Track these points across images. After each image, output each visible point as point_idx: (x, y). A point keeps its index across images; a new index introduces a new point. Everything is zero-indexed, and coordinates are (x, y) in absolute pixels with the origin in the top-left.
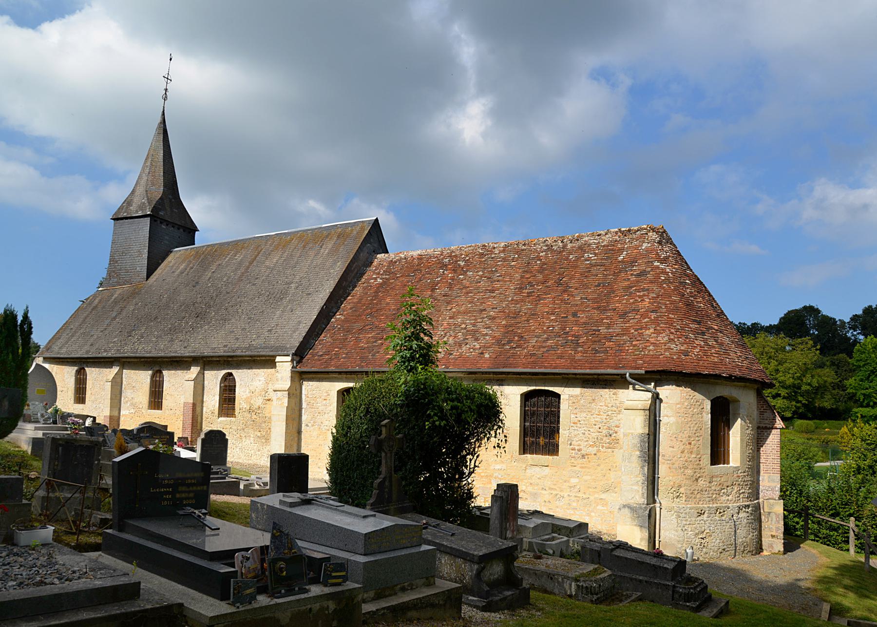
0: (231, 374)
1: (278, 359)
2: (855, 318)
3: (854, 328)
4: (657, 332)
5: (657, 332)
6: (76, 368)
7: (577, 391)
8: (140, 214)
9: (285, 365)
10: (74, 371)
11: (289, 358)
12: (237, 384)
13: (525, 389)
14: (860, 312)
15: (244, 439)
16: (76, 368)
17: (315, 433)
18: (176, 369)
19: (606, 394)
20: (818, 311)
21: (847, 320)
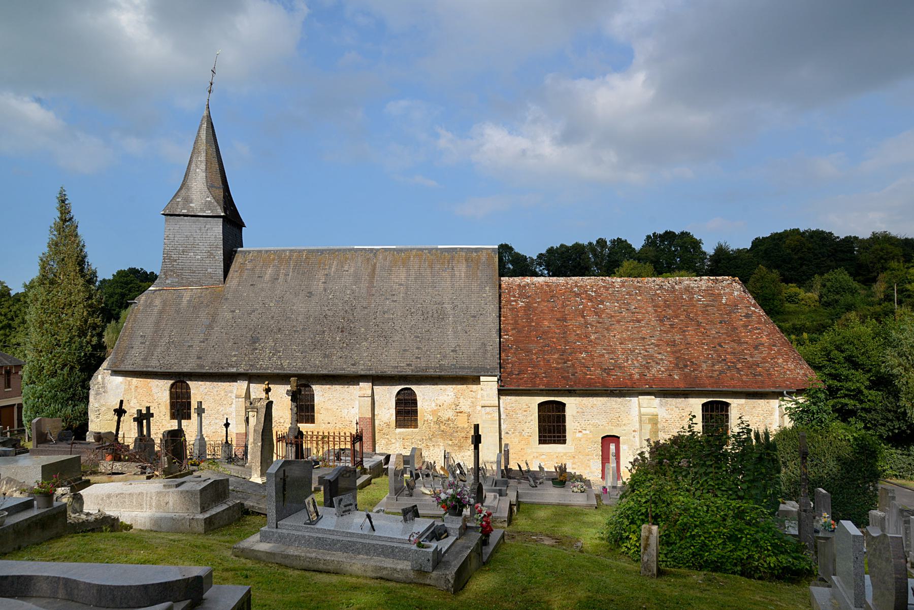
0: (413, 393)
1: (482, 378)
2: (540, 256)
3: (540, 264)
4: (786, 361)
5: (786, 361)
6: (172, 382)
7: (743, 401)
8: (208, 213)
9: (489, 385)
10: (169, 385)
11: (496, 379)
12: (418, 398)
13: (705, 400)
14: (544, 252)
15: (432, 448)
16: (172, 382)
17: (516, 440)
18: (332, 384)
19: (762, 402)
20: (511, 249)
21: (535, 258)
